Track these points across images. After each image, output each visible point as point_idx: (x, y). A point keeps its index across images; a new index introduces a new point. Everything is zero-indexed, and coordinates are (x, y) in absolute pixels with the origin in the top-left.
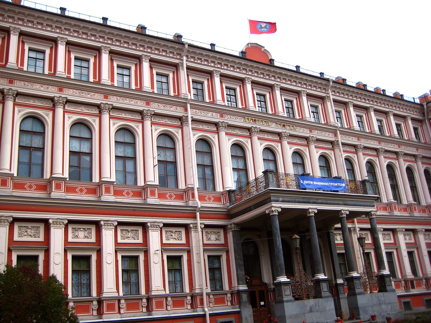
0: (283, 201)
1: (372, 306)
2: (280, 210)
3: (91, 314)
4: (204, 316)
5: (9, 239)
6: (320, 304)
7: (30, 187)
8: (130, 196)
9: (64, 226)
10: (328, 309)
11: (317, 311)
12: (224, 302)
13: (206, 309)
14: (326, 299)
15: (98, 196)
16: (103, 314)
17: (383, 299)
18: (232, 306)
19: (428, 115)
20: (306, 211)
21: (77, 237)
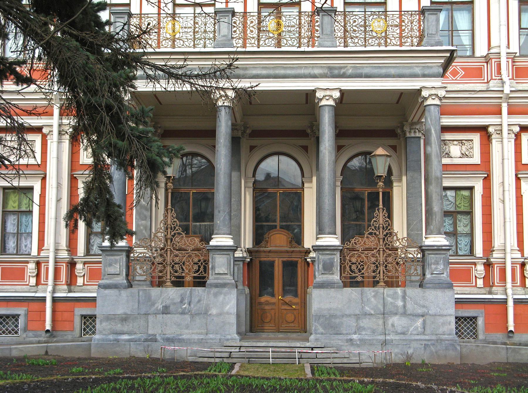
1: (358, 317)
3: (86, 283)
4: (505, 302)
5: (46, 162)
6: (195, 300)
8: (458, 77)
9: (513, 136)
10: (214, 311)
11: (183, 313)
12: (469, 280)
13: (510, 291)
14: (214, 290)
15: (486, 81)
16: (493, 286)
17: (400, 303)
18: (488, 289)
20: (310, 95)
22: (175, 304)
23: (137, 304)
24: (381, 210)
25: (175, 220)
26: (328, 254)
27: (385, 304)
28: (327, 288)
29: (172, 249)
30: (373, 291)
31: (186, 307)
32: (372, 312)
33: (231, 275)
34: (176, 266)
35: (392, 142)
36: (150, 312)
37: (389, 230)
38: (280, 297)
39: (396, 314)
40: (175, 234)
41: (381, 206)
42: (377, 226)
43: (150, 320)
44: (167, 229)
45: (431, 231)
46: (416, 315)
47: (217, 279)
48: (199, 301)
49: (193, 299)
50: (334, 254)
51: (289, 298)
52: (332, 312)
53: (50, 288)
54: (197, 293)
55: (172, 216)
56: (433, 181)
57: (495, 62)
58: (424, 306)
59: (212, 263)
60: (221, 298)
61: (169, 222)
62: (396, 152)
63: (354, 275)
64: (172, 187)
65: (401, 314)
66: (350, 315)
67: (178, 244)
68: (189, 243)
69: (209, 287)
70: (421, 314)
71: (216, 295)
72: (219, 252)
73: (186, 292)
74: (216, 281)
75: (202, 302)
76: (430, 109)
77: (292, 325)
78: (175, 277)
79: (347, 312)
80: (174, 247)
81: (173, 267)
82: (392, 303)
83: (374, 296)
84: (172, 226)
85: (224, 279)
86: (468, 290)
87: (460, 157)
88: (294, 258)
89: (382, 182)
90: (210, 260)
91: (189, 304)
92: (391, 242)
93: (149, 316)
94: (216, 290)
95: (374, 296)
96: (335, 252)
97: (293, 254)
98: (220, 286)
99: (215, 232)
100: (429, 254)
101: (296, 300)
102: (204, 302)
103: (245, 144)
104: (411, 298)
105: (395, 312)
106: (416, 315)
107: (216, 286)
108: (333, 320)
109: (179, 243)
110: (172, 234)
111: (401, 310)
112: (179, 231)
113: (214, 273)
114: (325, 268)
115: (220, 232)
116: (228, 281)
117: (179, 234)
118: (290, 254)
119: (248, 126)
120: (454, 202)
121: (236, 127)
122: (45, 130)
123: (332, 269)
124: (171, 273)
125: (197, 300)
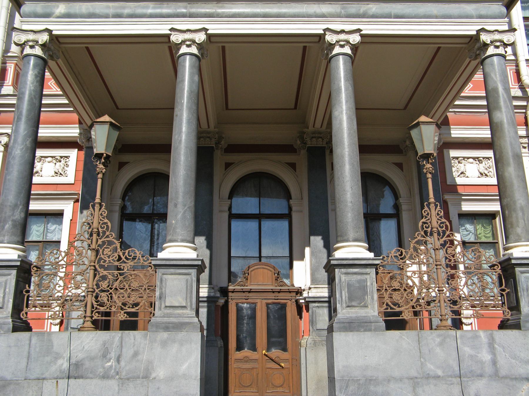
6: (128, 353)
10: (160, 373)
11: (105, 376)
17: (486, 357)
22: (92, 359)
23: (25, 360)
24: (432, 206)
25: (106, 221)
26: (355, 273)
27: (461, 359)
28: (358, 331)
29: (97, 267)
30: (439, 336)
31: (111, 366)
32: (440, 373)
33: (192, 309)
34: (103, 294)
35: (397, 158)
36: (47, 375)
37: (448, 236)
38: (264, 352)
39: (481, 376)
40: (104, 243)
41: (432, 200)
42: (429, 229)
43: (45, 391)
44: (91, 235)
45: (518, 235)
46: (516, 379)
47: (169, 316)
48: (136, 354)
49: (124, 350)
50: (367, 274)
51: (275, 353)
52: (369, 373)
54: (132, 341)
55: (101, 215)
56: (511, 161)
57: (510, 70)
59: (161, 289)
60: (174, 349)
61: (95, 225)
62: (402, 170)
63: (397, 309)
64: (104, 171)
65: (490, 376)
66: (401, 380)
67: (107, 259)
68: (126, 258)
69: (154, 329)
70: (524, 376)
71: (164, 344)
72: (172, 270)
73: (114, 337)
74: (166, 320)
75: (140, 357)
76: (493, 61)
77: (281, 389)
78: (98, 313)
79: (397, 374)
80: (102, 263)
81: (96, 297)
82: (471, 356)
83: (441, 344)
84: (100, 229)
85: (180, 316)
87: (479, 177)
88: (282, 298)
89: (431, 164)
90: (158, 283)
91: (118, 360)
92: (453, 256)
93: (45, 382)
94: (165, 335)
95: (441, 344)
96: (368, 270)
97: (281, 294)
98: (174, 328)
99: (169, 238)
100: (522, 272)
101: (284, 355)
102: (144, 357)
103: (219, 159)
104: (504, 348)
105: (479, 372)
106: (516, 379)
107: (167, 327)
108: (372, 388)
109: (109, 257)
110: (100, 242)
111: (489, 369)
112: (111, 239)
113: (163, 306)
114: (351, 298)
115: (175, 238)
116: (187, 320)
117: (110, 243)
118: (277, 294)
119: (224, 136)
120: (473, 232)
121: (208, 135)
123: (364, 299)
124: (93, 307)
125: (131, 352)
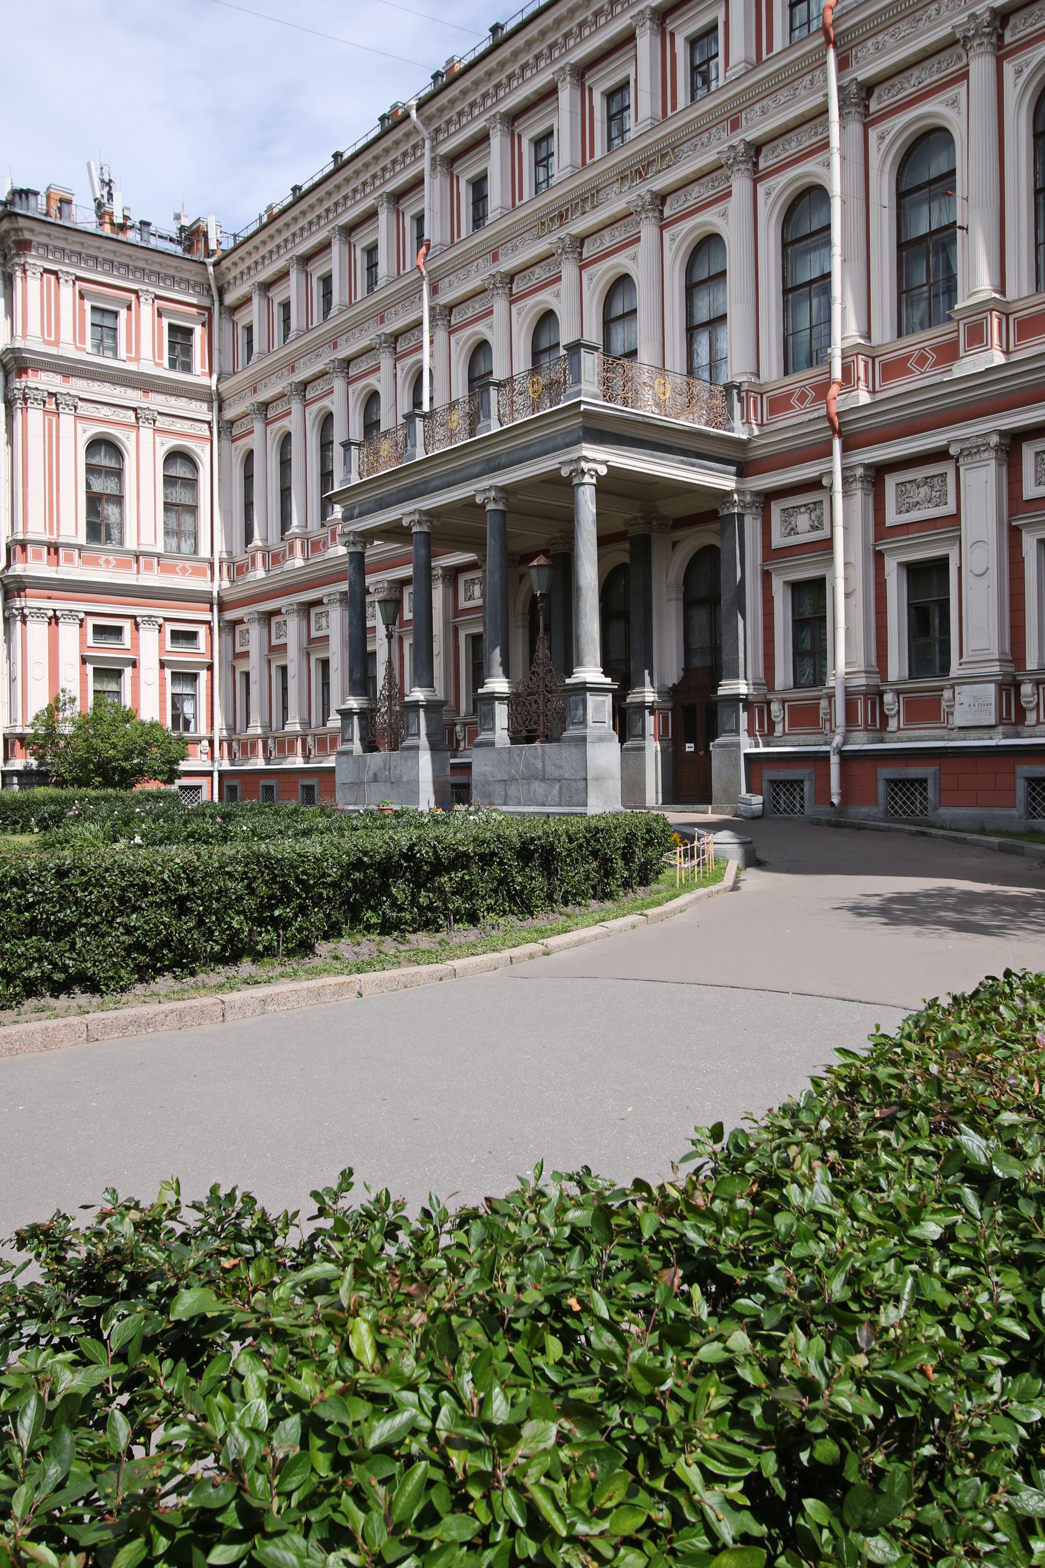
0: (360, 515)
2: (603, 470)
4: (825, 757)
7: (922, 360)
10: (405, 779)
19: (221, 292)
20: (469, 505)
21: (793, 531)
53: (837, 740)
58: (560, 767)
86: (813, 738)
122: (825, 482)
